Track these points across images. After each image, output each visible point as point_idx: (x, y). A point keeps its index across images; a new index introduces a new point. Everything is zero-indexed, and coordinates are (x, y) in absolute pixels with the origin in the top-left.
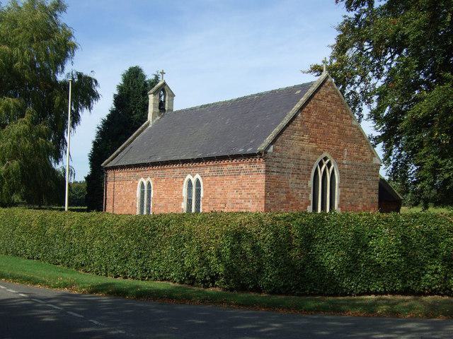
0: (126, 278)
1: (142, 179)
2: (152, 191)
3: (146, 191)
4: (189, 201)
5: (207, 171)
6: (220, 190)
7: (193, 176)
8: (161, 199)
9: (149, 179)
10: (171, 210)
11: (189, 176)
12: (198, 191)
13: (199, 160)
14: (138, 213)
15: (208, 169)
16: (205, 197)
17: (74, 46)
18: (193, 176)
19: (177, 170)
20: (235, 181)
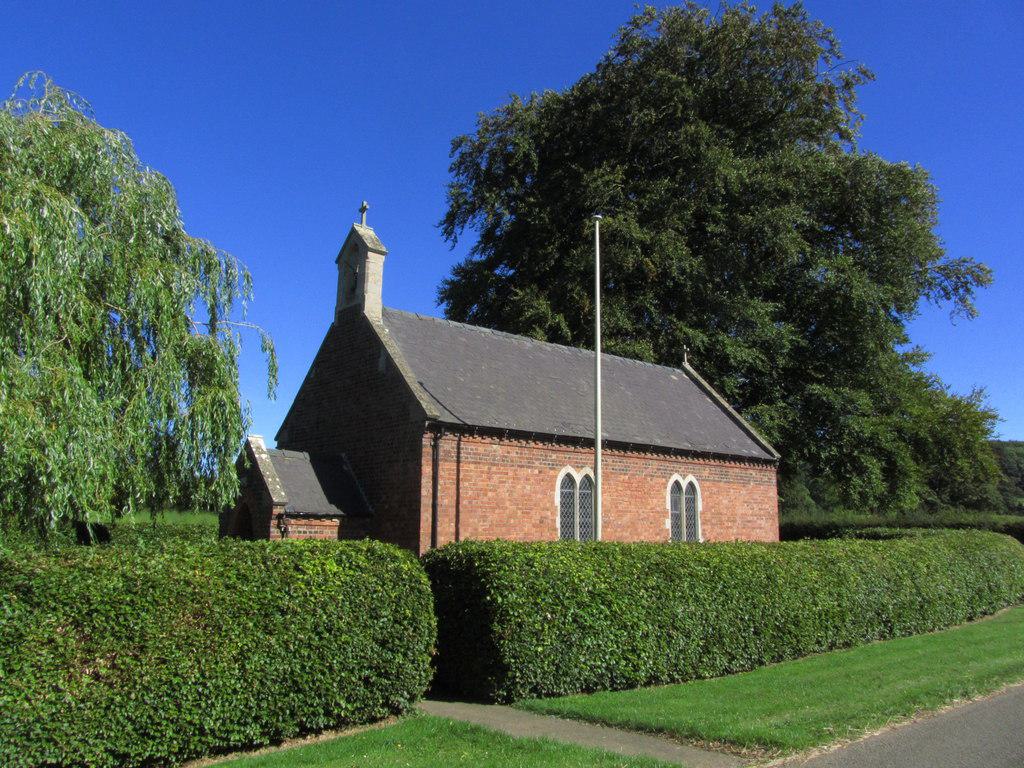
0: (276, 741)
1: (570, 469)
2: (668, 506)
3: (684, 497)
4: (676, 518)
5: (706, 473)
6: (725, 502)
7: (684, 477)
8: (621, 513)
9: (691, 478)
10: (646, 536)
11: (676, 477)
12: (691, 502)
13: (704, 455)
14: (336, 521)
15: (708, 469)
16: (706, 508)
17: (466, 164)
18: (684, 477)
19: (654, 463)
20: (743, 492)
